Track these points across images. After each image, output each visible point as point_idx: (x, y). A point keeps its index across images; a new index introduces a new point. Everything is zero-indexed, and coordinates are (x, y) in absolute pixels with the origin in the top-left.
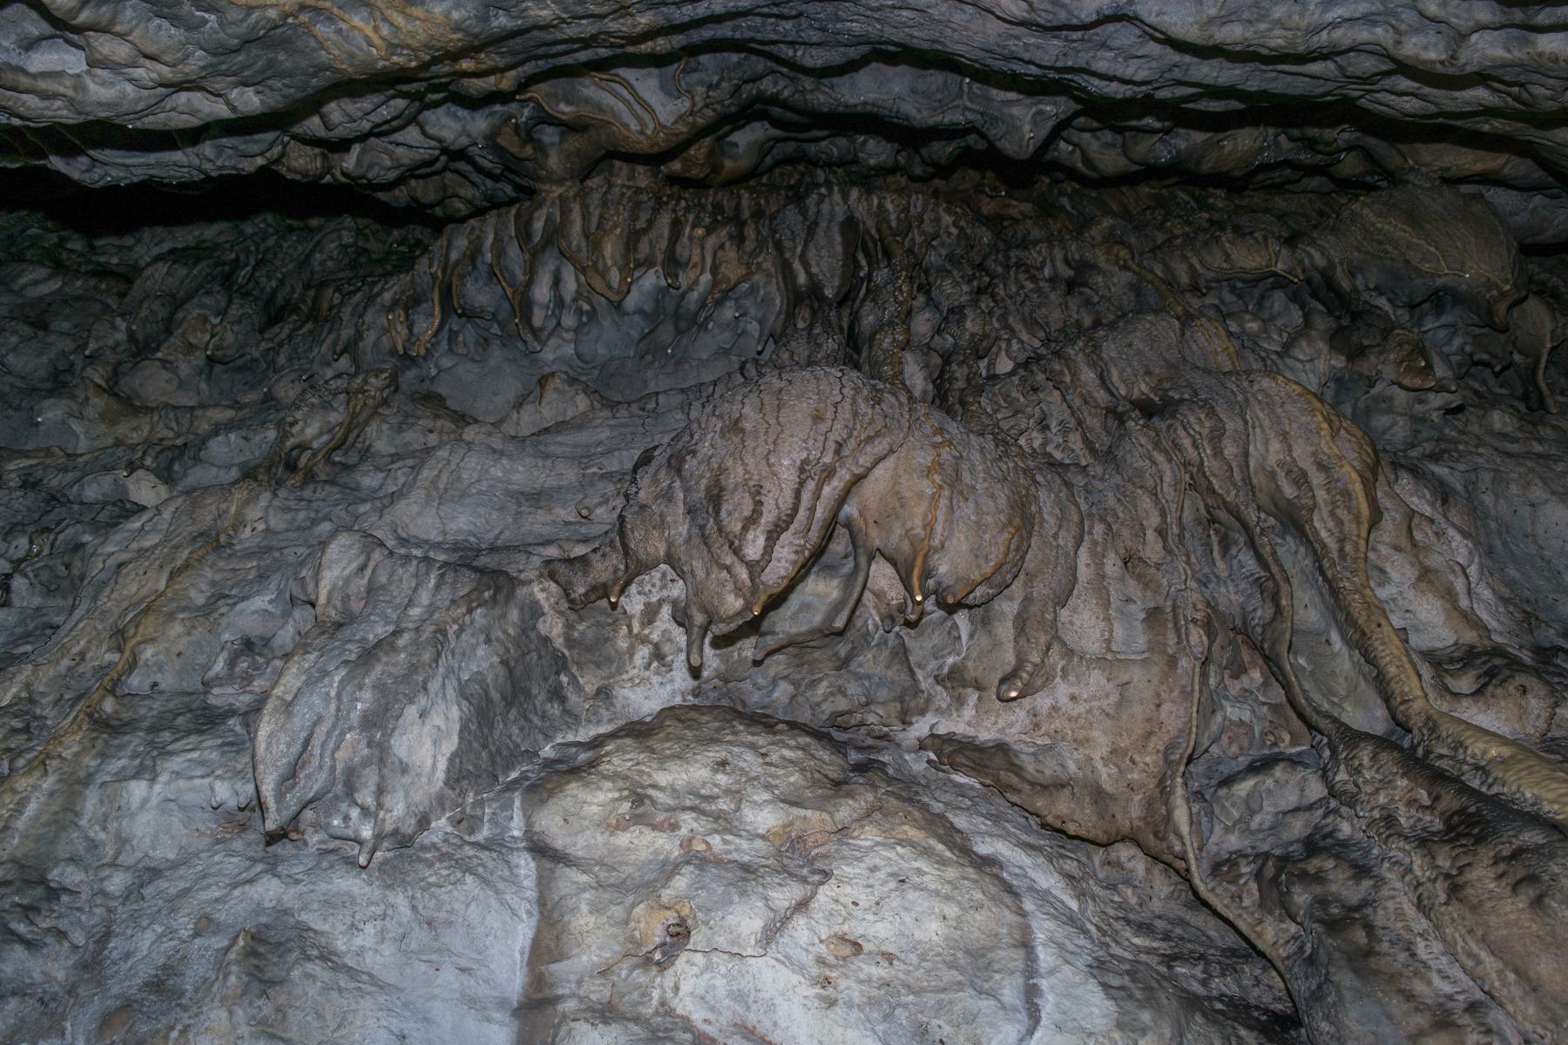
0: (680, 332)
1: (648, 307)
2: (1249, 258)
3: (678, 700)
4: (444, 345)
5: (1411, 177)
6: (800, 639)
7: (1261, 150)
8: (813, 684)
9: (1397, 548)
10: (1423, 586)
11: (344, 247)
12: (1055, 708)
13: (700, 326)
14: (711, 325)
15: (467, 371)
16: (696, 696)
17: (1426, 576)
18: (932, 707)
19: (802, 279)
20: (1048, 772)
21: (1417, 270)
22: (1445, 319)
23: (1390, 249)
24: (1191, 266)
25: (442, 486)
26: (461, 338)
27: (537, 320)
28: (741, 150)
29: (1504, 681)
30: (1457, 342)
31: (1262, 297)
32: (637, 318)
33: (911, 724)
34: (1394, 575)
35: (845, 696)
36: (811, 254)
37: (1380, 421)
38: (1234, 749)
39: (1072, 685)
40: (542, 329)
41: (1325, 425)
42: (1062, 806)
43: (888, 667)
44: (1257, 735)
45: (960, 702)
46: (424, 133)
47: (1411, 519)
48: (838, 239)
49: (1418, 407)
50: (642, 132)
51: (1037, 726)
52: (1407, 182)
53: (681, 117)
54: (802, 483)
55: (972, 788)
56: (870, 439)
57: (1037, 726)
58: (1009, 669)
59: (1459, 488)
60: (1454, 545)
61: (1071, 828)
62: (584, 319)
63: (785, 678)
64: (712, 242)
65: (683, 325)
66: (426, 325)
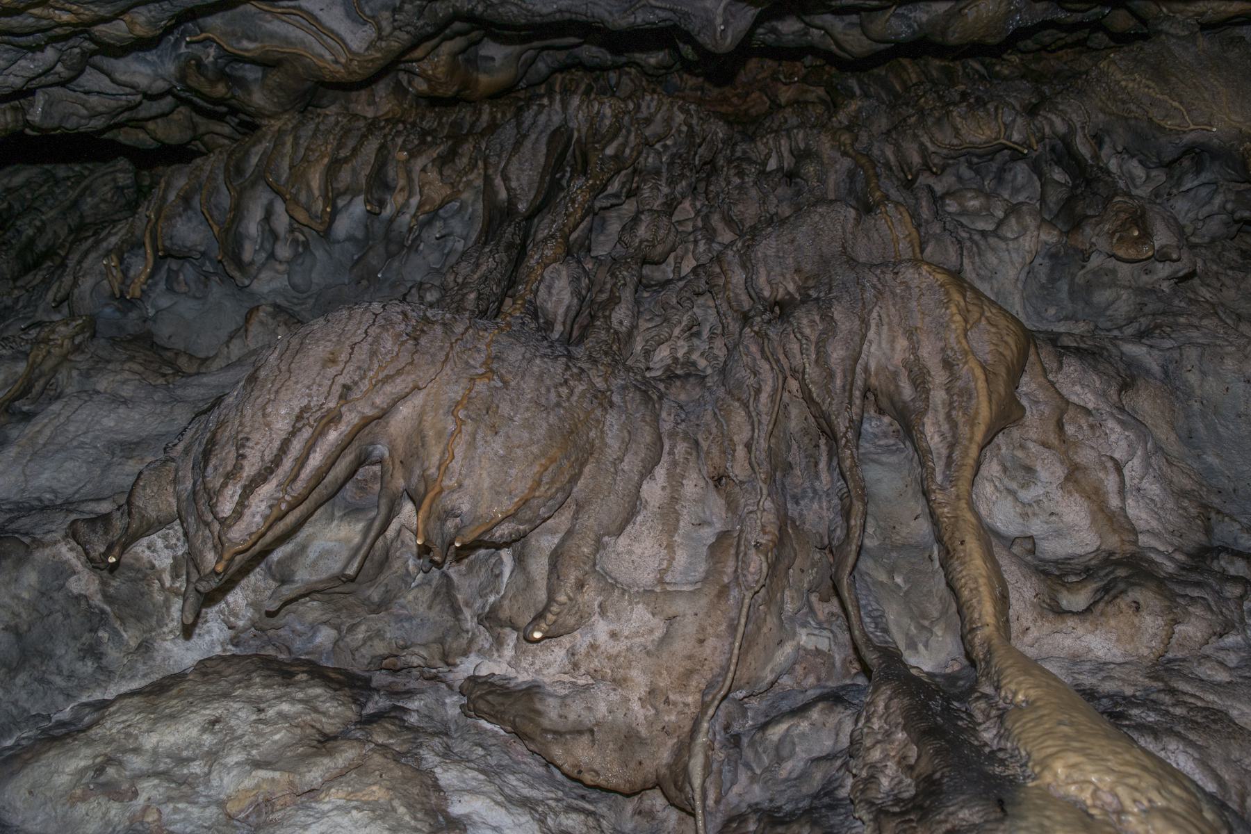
0: (390, 256)
1: (359, 234)
2: (979, 132)
3: (218, 650)
4: (162, 286)
5: (1165, 26)
6: (320, 586)
7: (1009, 14)
8: (352, 628)
9: (1044, 444)
10: (1070, 486)
11: (120, 189)
12: (593, 647)
13: (410, 248)
14: (421, 247)
15: (188, 308)
16: (236, 645)
17: (1074, 476)
18: (475, 647)
19: (503, 195)
20: (572, 717)
21: (1161, 128)
22: (1205, 177)
23: (1133, 107)
24: (922, 144)
25: (41, 442)
26: (181, 277)
27: (247, 256)
28: (497, 63)
29: (1115, 597)
30: (1218, 200)
31: (1002, 170)
32: (348, 245)
33: (455, 665)
34: (1043, 474)
35: (383, 639)
36: (513, 169)
37: (1102, 296)
38: (811, 680)
39: (612, 621)
40: (251, 263)
41: (958, 318)
42: (583, 753)
43: (430, 607)
44: (838, 664)
45: (499, 642)
46: (113, 81)
47: (1063, 412)
48: (544, 149)
49: (1145, 278)
50: (336, 62)
51: (576, 666)
52: (1160, 32)
53: (371, 43)
54: (294, 433)
55: (495, 735)
56: (389, 378)
57: (576, 666)
58: (540, 607)
59: (1156, 368)
60: (1113, 437)
61: (588, 778)
62: (301, 249)
63: (324, 623)
64: (419, 163)
65: (393, 248)
66: (140, 267)
